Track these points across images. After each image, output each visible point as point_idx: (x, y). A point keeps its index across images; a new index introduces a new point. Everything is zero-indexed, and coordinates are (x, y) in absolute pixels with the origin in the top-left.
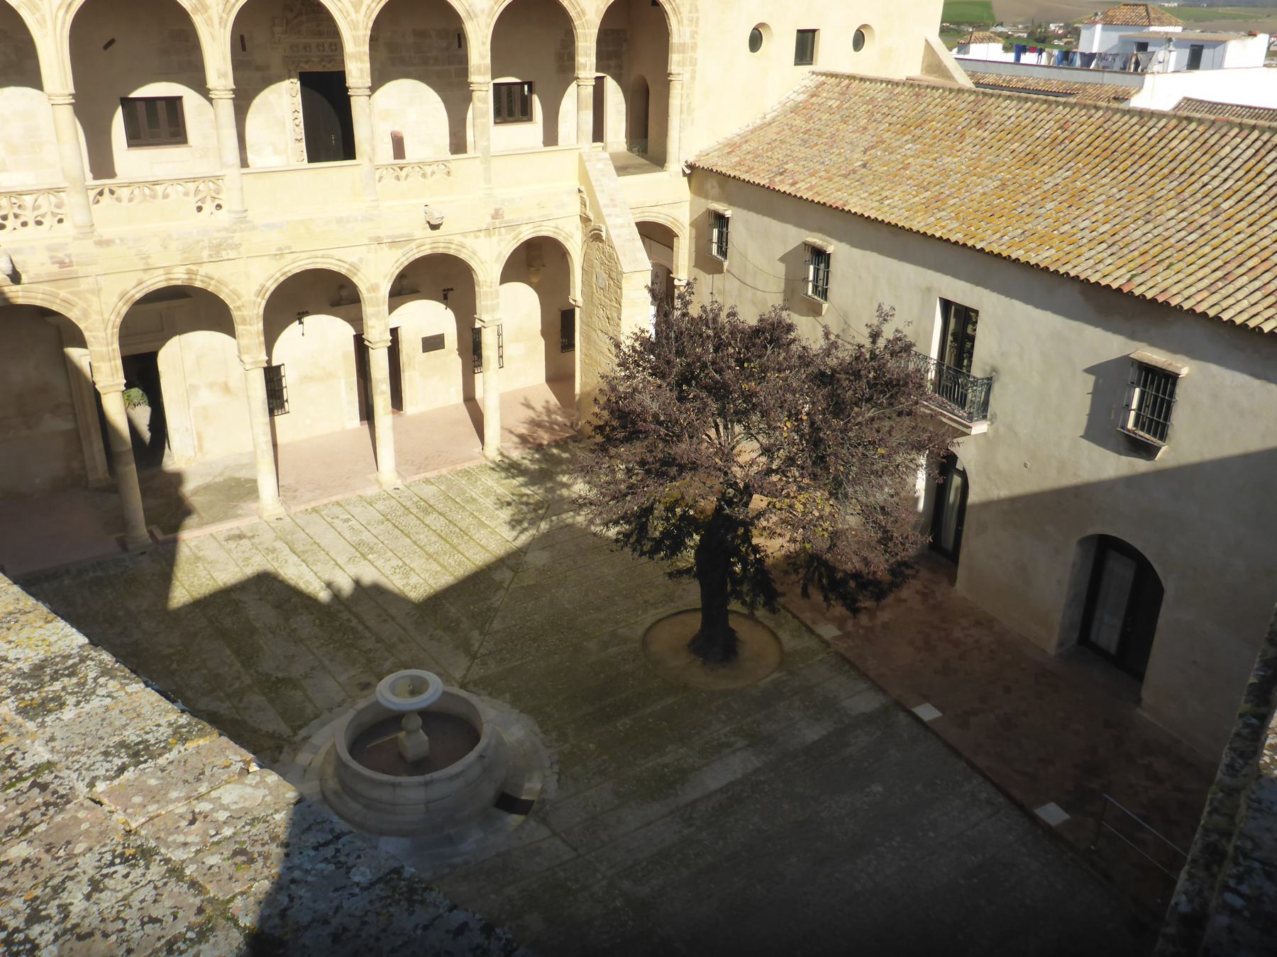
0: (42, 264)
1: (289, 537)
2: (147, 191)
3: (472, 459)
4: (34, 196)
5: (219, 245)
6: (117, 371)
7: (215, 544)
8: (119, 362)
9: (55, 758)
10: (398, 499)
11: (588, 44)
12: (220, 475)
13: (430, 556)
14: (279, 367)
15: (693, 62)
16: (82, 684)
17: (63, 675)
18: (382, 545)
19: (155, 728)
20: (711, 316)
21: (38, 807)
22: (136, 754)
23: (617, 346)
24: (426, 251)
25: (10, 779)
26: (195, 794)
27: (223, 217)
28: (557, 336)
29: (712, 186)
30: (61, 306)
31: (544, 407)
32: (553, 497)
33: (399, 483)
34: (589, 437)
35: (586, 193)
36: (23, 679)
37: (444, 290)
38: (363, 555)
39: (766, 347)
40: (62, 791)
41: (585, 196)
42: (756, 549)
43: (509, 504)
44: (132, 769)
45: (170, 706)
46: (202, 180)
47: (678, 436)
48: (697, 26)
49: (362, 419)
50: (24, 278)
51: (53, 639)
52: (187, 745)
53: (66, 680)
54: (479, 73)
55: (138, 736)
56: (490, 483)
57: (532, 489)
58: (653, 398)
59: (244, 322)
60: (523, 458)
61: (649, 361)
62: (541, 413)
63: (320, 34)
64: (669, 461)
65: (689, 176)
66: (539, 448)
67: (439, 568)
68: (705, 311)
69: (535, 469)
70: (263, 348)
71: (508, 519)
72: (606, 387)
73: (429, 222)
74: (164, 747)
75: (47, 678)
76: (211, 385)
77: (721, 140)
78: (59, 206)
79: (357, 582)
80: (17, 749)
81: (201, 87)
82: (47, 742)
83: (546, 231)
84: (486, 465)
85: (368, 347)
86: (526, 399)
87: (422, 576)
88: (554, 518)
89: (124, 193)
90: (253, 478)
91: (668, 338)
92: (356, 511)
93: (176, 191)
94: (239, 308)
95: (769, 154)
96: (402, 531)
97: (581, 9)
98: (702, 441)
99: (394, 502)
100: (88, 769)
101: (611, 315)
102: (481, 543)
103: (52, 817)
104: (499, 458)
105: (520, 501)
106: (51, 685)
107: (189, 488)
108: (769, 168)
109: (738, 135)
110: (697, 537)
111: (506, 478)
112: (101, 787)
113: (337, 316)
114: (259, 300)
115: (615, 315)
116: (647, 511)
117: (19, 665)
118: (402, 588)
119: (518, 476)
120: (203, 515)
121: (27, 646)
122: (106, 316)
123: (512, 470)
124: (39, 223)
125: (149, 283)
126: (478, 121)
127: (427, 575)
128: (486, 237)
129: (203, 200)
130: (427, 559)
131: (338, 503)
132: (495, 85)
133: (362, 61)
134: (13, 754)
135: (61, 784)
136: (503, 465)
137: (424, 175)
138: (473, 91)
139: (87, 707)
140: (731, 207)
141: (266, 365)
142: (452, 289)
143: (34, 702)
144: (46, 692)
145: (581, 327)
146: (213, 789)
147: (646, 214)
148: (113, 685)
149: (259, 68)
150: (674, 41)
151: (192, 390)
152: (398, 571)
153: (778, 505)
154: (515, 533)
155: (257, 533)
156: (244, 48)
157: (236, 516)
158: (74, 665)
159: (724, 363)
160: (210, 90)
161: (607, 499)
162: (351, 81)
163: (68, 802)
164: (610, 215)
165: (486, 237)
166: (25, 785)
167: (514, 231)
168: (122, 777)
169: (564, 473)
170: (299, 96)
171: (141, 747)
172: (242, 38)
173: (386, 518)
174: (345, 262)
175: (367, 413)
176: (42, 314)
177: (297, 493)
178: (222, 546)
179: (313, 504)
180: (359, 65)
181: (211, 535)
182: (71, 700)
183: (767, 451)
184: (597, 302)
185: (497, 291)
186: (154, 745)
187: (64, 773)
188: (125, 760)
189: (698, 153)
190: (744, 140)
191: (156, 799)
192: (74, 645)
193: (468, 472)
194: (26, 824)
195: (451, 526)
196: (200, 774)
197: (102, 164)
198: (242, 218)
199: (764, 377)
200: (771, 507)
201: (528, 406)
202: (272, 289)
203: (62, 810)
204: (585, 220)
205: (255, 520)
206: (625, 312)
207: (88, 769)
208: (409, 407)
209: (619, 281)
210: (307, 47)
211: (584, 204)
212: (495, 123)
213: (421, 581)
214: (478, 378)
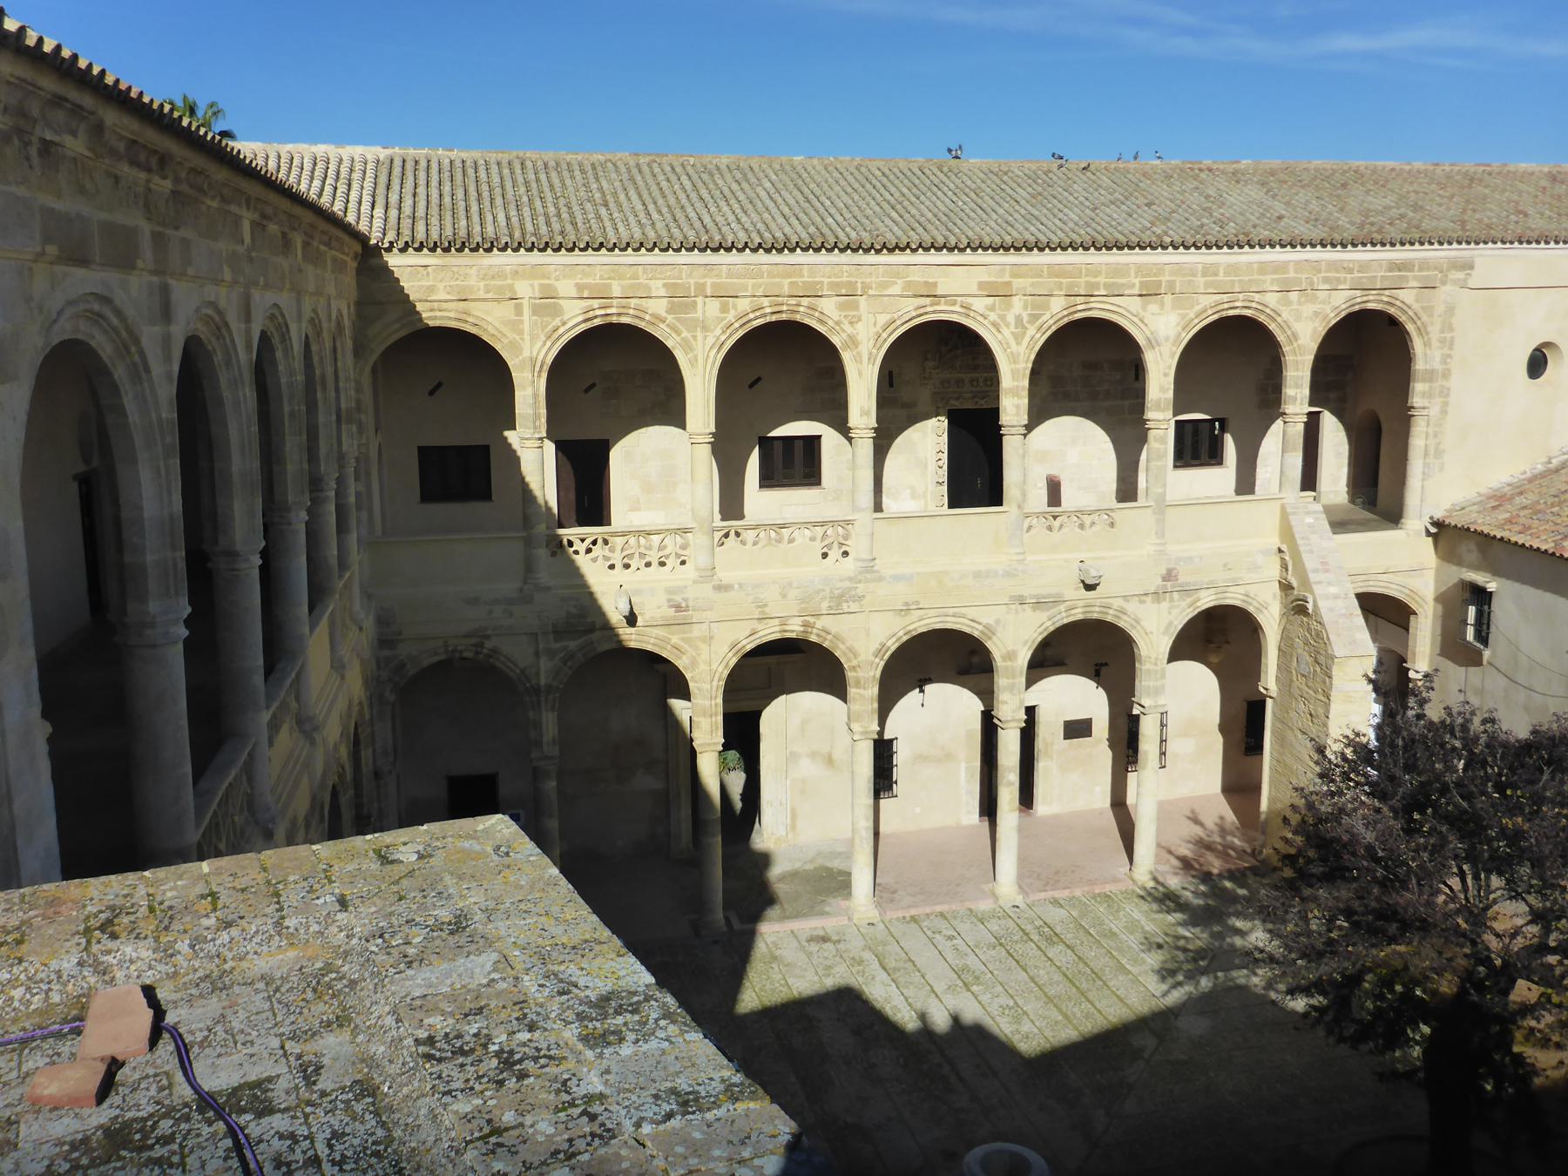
0: (659, 607)
1: (880, 948)
2: (773, 534)
3: (1115, 880)
4: (662, 536)
5: (841, 596)
6: (717, 728)
7: (795, 944)
8: (720, 718)
9: (607, 1092)
10: (1016, 920)
11: (1300, 374)
12: (812, 861)
13: (1050, 999)
14: (891, 741)
15: (1445, 393)
16: (644, 1023)
17: (626, 1011)
18: (990, 975)
19: (707, 1081)
20: (1460, 720)
21: (585, 1136)
22: (685, 1104)
23: (1321, 750)
24: (1078, 615)
25: (564, 1103)
26: (738, 1157)
27: (849, 565)
28: (1240, 734)
29: (1469, 550)
30: (671, 653)
31: (1216, 824)
32: (1221, 947)
33: (1019, 900)
34: (1275, 869)
35: (1288, 553)
36: (590, 1008)
37: (1096, 665)
38: (965, 984)
39: (1542, 772)
40: (609, 1126)
41: (1287, 558)
42: (1519, 1059)
43: (1160, 946)
44: (679, 1117)
45: (726, 1062)
46: (831, 524)
47: (1401, 881)
48: (1451, 348)
49: (982, 814)
50: (640, 622)
51: (621, 973)
52: (736, 1105)
53: (629, 1016)
54: (1158, 408)
55: (690, 1085)
56: (1137, 915)
57: (1192, 930)
58: (1367, 826)
59: (858, 684)
60: (1184, 888)
61: (1366, 775)
62: (1212, 832)
63: (975, 368)
64: (1388, 914)
65: (1435, 537)
66: (1206, 877)
67: (1061, 1018)
68: (1450, 714)
69: (1199, 906)
70: (876, 716)
71: (1156, 967)
72: (1301, 802)
73: (1083, 581)
74: (714, 1103)
75: (611, 1011)
76: (813, 755)
77: (1483, 490)
78: (684, 547)
79: (956, 1019)
80: (574, 1075)
81: (843, 428)
82: (602, 1073)
83: (1233, 598)
84: (1134, 891)
85: (997, 726)
86: (1193, 812)
87: (1037, 1024)
88: (1220, 974)
89: (749, 536)
90: (847, 870)
91: (1393, 745)
92: (964, 927)
93: (803, 536)
94: (854, 668)
95: (1556, 509)
96: (1018, 962)
97: (1293, 333)
98: (1439, 891)
99: (1011, 924)
100: (636, 1109)
101: (1316, 711)
102: (1118, 993)
103: (596, 1149)
104: (1151, 884)
105: (1177, 945)
106: (614, 1018)
107: (775, 872)
108: (1554, 528)
109: (1509, 485)
110: (1426, 1029)
111: (1159, 912)
112: (646, 1129)
113: (963, 686)
114: (877, 660)
115: (1321, 711)
116: (1354, 980)
117: (588, 992)
118: (1010, 1035)
119: (1175, 911)
120: (786, 906)
121: (597, 976)
122: (714, 667)
123: (1168, 902)
124: (662, 564)
125: (761, 633)
126: (1153, 464)
127: (1044, 1023)
128: (1153, 602)
129: (829, 546)
130: (1046, 1003)
131: (942, 915)
132: (1177, 422)
133: (1019, 397)
134: (570, 1079)
135: (610, 1118)
136: (1156, 894)
137: (1082, 526)
138: (1149, 429)
139: (645, 1047)
140: (1496, 578)
141: (876, 737)
142: (1106, 664)
143: (596, 1032)
144: (609, 1024)
145: (1273, 725)
146: (756, 1156)
147: (1371, 583)
148: (673, 1029)
149: (907, 405)
150: (1417, 367)
151: (792, 758)
152: (1007, 1012)
153: (1555, 999)
154: (1164, 987)
155: (843, 938)
156: (891, 385)
157: (822, 914)
158: (639, 1003)
159: (1476, 786)
160: (850, 429)
161: (1293, 956)
162: (1004, 419)
163: (614, 1137)
164: (1319, 583)
165: (1153, 602)
166: (576, 1111)
167: (1189, 596)
168: (668, 1123)
169: (1238, 915)
171: (691, 1097)
172: (891, 374)
173: (999, 941)
174: (979, 623)
175: (989, 807)
176: (652, 660)
177: (895, 895)
178: (802, 948)
179: (913, 912)
181: (792, 932)
182: (631, 1037)
183: (1537, 917)
184: (1296, 692)
185: (1163, 671)
186: (704, 1098)
187: (614, 1108)
188: (674, 1107)
189: (1448, 506)
190: (1518, 490)
191: (699, 1153)
192: (641, 983)
193: (1109, 896)
194: (571, 1150)
195: (1081, 965)
196: (746, 1138)
197: (731, 505)
198: (869, 569)
199: (1537, 812)
200: (1544, 1002)
201: (1196, 821)
202: (893, 648)
203: (606, 1144)
204: (1286, 587)
205: (844, 921)
206: (1335, 708)
207: (636, 1109)
208: (1042, 807)
209: (1329, 668)
210: (959, 382)
211: (1285, 567)
212: (1175, 467)
213: (1036, 1030)
214: (1132, 778)
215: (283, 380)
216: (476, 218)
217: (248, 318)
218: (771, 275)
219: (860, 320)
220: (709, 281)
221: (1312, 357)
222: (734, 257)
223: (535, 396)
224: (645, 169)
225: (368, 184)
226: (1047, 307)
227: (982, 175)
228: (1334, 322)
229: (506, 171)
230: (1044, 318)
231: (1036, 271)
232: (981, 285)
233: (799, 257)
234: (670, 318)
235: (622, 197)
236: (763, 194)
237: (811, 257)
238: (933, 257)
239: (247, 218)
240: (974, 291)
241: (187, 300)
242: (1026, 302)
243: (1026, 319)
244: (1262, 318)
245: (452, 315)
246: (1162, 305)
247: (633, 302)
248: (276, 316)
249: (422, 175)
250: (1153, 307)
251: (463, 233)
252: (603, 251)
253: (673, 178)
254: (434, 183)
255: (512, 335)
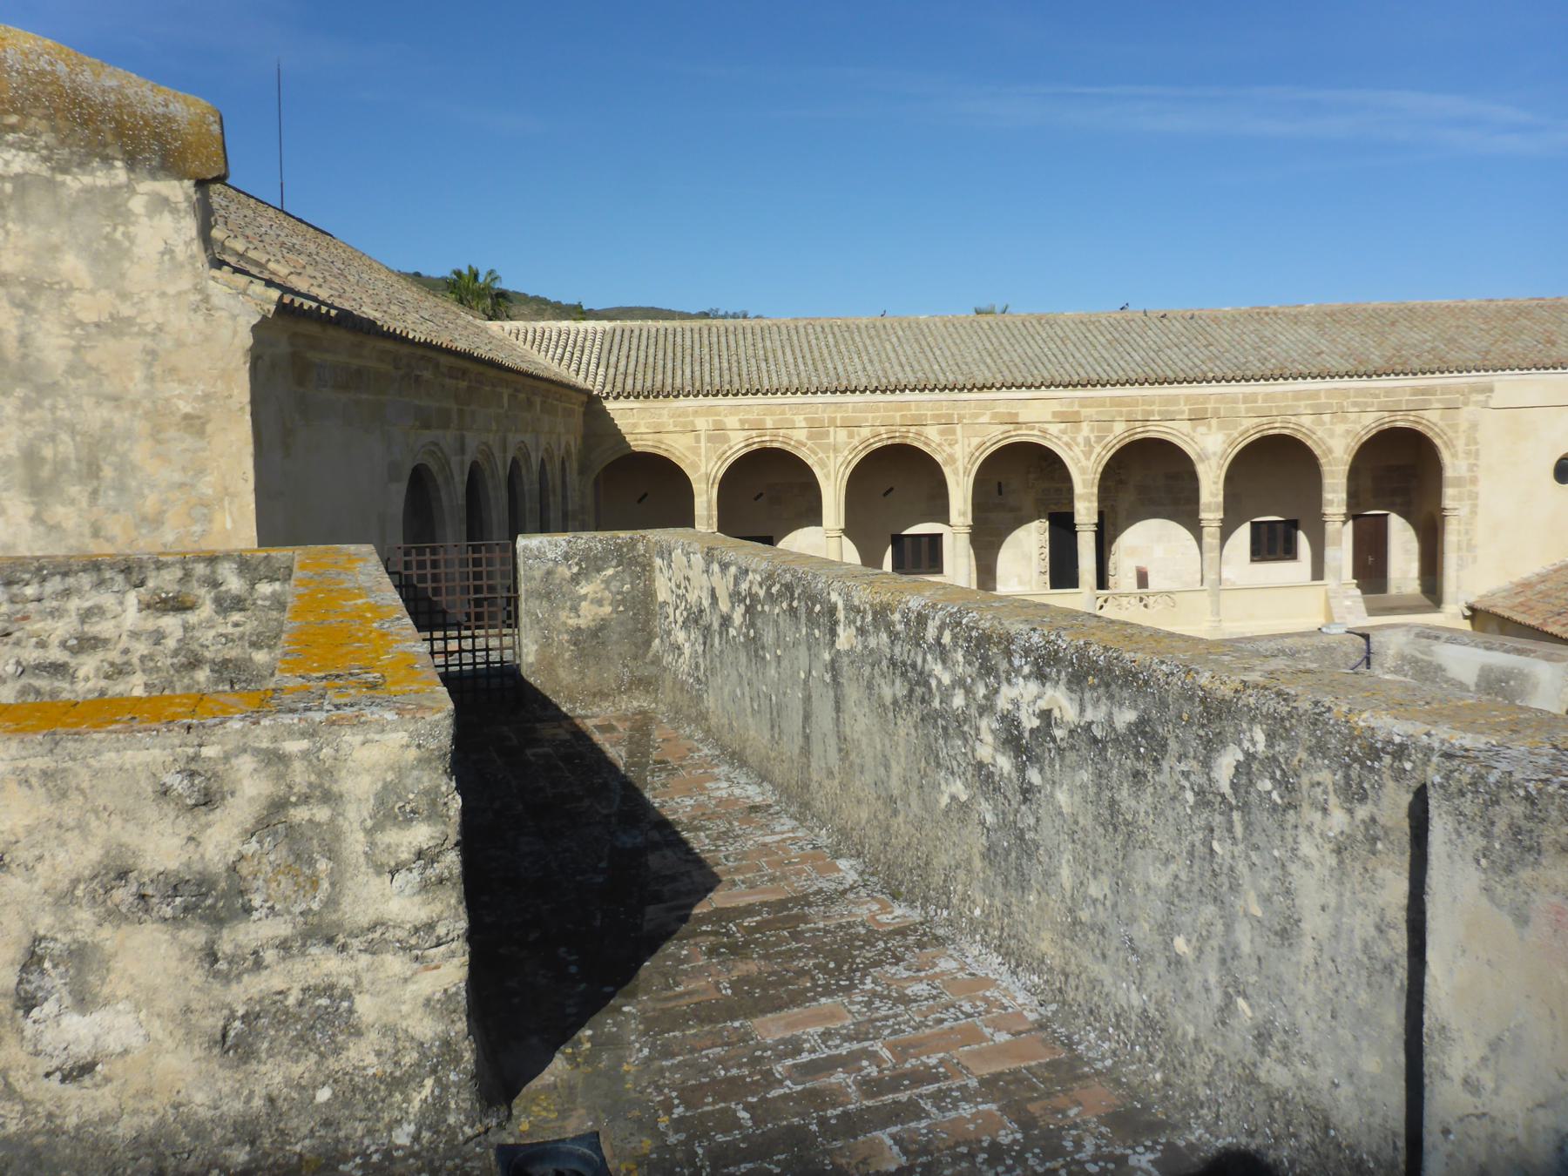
15: (1474, 496)
48: (1477, 459)
133: (1090, 501)
162: (1078, 519)
170: (1047, 534)
180: (1087, 504)
215: (526, 488)
216: (669, 373)
217: (505, 451)
218: (886, 410)
219: (956, 442)
220: (839, 415)
221: (1347, 467)
222: (857, 397)
223: (709, 502)
224: (802, 331)
225: (596, 350)
226: (1110, 430)
227: (1072, 326)
228: (1365, 438)
229: (696, 336)
230: (1108, 439)
231: (1100, 403)
232: (1055, 414)
233: (908, 396)
234: (809, 443)
235: (779, 353)
236: (889, 347)
237: (917, 396)
238: (1015, 394)
239: (506, 393)
240: (1049, 418)
241: (473, 441)
242: (1093, 426)
243: (1093, 439)
244: (1299, 436)
245: (650, 443)
246: (1209, 427)
247: (782, 432)
248: (523, 448)
249: (635, 341)
250: (1202, 429)
251: (658, 384)
252: (760, 395)
253: (821, 336)
254: (643, 347)
255: (691, 457)
